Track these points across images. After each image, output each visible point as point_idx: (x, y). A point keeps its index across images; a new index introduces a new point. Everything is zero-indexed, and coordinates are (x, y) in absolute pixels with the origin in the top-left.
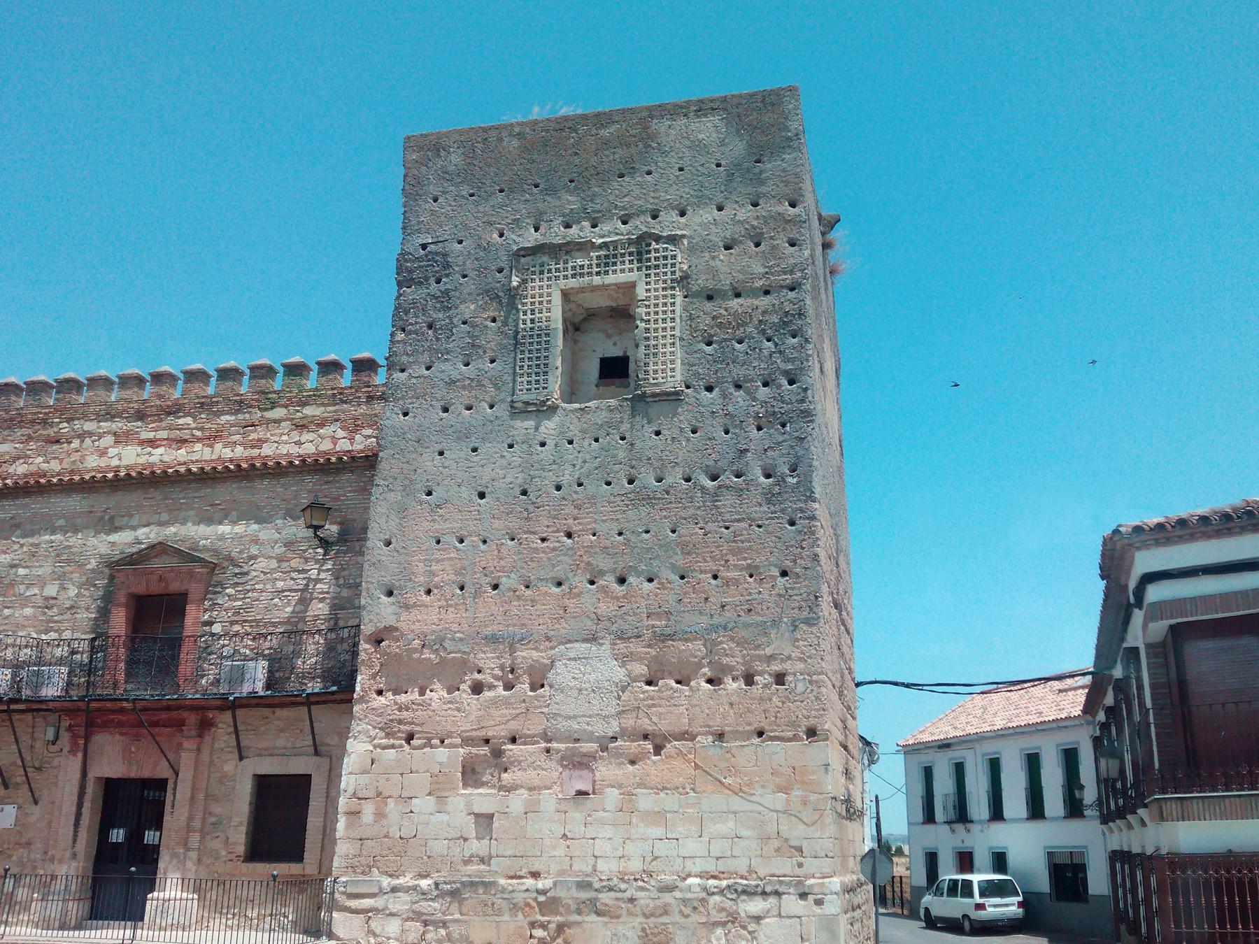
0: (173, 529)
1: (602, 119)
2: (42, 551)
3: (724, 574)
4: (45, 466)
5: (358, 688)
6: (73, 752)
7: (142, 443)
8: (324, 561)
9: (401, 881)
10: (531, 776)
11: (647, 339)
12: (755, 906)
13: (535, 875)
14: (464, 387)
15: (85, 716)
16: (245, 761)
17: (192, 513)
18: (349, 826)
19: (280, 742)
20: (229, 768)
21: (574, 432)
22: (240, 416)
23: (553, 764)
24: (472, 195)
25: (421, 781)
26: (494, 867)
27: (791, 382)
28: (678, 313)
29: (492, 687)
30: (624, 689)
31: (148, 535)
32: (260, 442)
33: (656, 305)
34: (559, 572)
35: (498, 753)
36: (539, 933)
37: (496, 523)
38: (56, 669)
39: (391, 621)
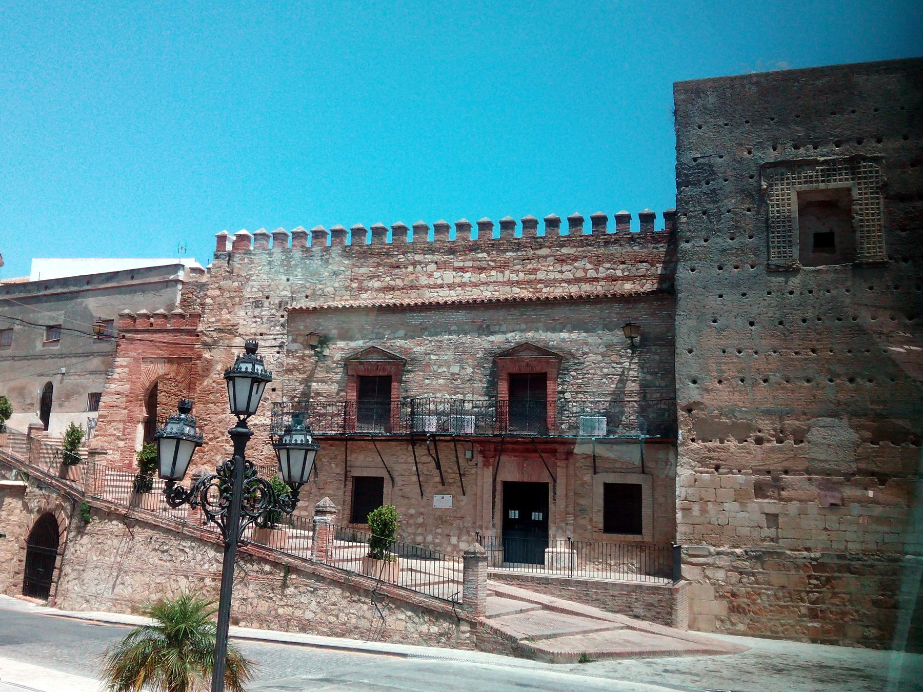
0: (530, 334)
4: (392, 283)
5: (680, 438)
7: (455, 269)
8: (632, 358)
10: (801, 494)
11: (862, 226)
13: (808, 549)
14: (732, 254)
15: (490, 447)
16: (598, 475)
17: (540, 324)
18: (684, 516)
20: (587, 478)
21: (812, 285)
22: (520, 253)
24: (726, 125)
28: (882, 209)
29: (769, 441)
30: (858, 446)
31: (515, 337)
32: (534, 271)
34: (810, 373)
35: (776, 480)
36: (814, 582)
37: (764, 342)
38: (467, 417)
39: (698, 398)
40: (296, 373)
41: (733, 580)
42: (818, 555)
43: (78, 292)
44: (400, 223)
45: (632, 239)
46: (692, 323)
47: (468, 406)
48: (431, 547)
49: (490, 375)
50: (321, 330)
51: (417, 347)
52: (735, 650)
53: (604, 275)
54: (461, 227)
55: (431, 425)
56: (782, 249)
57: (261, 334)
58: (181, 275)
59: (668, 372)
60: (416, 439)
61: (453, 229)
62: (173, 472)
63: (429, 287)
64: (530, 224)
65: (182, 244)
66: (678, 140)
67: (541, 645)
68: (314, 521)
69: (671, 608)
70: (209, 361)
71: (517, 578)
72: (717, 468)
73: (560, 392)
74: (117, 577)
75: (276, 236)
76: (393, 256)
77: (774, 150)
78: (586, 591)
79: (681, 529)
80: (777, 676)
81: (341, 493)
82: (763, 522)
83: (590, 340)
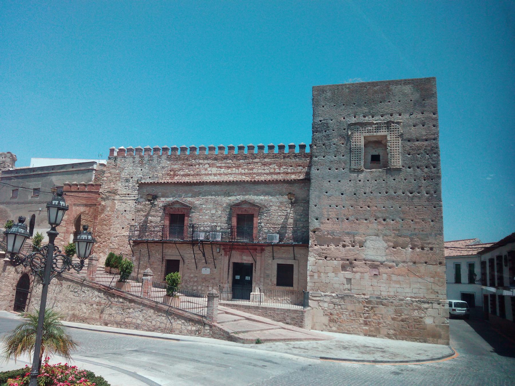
1: (374, 84)
2: (209, 201)
3: (415, 220)
5: (310, 244)
6: (226, 255)
7: (217, 167)
8: (291, 208)
9: (327, 293)
10: (361, 270)
12: (426, 306)
13: (364, 294)
15: (228, 247)
17: (252, 193)
18: (310, 279)
19: (284, 256)
23: (367, 267)
25: (329, 269)
26: (352, 292)
27: (434, 167)
29: (348, 246)
31: (240, 198)
32: (252, 169)
33: (393, 142)
34: (366, 216)
35: (351, 263)
36: (366, 309)
37: (347, 202)
38: (217, 233)
39: (318, 226)
40: (142, 212)
41: (331, 308)
42: (368, 297)
43: (48, 173)
44: (193, 146)
45: (296, 156)
46: (317, 193)
47: (218, 228)
48: (200, 292)
49: (229, 214)
50: (154, 193)
51: (197, 201)
52: (329, 339)
53: (282, 172)
54: (221, 148)
55: (202, 237)
56: (356, 162)
57: (128, 194)
58: (95, 167)
59: (306, 214)
60: (194, 243)
61: (217, 149)
62: (13, 250)
63: (205, 175)
64: (251, 148)
65: (101, 153)
66: (314, 112)
67: (241, 336)
68: (143, 279)
69: (302, 320)
70: (104, 206)
71: (236, 305)
72: (326, 258)
73: (259, 223)
74: (54, 303)
75: (137, 150)
76: (190, 160)
77: (355, 117)
78: (266, 312)
79: (309, 285)
80: (343, 350)
81: (160, 267)
82: (345, 281)
83: (273, 200)
